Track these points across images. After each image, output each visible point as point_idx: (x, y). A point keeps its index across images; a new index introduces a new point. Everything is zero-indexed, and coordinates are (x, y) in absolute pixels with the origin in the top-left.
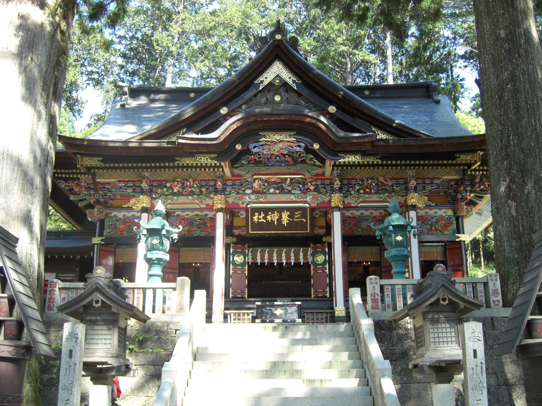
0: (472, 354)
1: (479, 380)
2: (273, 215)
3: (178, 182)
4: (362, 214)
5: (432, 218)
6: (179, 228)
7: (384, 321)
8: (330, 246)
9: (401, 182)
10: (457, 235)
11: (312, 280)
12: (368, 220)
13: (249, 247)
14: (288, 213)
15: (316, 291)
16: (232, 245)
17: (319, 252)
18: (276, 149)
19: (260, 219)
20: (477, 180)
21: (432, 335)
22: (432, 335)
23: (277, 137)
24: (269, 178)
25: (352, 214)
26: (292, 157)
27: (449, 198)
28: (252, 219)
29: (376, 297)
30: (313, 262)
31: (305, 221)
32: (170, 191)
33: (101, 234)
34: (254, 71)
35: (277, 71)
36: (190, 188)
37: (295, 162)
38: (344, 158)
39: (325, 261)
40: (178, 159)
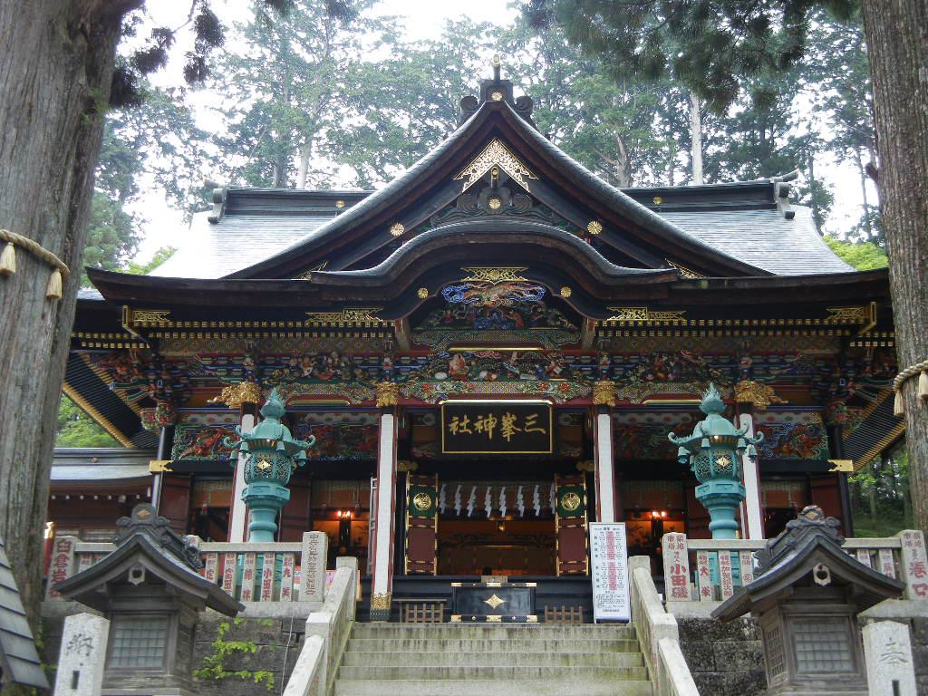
2: (485, 421)
3: (310, 357)
5: (782, 428)
6: (310, 440)
7: (696, 620)
8: (592, 479)
9: (724, 359)
10: (830, 461)
14: (514, 418)
18: (492, 297)
20: (868, 358)
23: (493, 276)
28: (447, 428)
29: (682, 573)
30: (559, 509)
31: (544, 432)
35: (495, 158)
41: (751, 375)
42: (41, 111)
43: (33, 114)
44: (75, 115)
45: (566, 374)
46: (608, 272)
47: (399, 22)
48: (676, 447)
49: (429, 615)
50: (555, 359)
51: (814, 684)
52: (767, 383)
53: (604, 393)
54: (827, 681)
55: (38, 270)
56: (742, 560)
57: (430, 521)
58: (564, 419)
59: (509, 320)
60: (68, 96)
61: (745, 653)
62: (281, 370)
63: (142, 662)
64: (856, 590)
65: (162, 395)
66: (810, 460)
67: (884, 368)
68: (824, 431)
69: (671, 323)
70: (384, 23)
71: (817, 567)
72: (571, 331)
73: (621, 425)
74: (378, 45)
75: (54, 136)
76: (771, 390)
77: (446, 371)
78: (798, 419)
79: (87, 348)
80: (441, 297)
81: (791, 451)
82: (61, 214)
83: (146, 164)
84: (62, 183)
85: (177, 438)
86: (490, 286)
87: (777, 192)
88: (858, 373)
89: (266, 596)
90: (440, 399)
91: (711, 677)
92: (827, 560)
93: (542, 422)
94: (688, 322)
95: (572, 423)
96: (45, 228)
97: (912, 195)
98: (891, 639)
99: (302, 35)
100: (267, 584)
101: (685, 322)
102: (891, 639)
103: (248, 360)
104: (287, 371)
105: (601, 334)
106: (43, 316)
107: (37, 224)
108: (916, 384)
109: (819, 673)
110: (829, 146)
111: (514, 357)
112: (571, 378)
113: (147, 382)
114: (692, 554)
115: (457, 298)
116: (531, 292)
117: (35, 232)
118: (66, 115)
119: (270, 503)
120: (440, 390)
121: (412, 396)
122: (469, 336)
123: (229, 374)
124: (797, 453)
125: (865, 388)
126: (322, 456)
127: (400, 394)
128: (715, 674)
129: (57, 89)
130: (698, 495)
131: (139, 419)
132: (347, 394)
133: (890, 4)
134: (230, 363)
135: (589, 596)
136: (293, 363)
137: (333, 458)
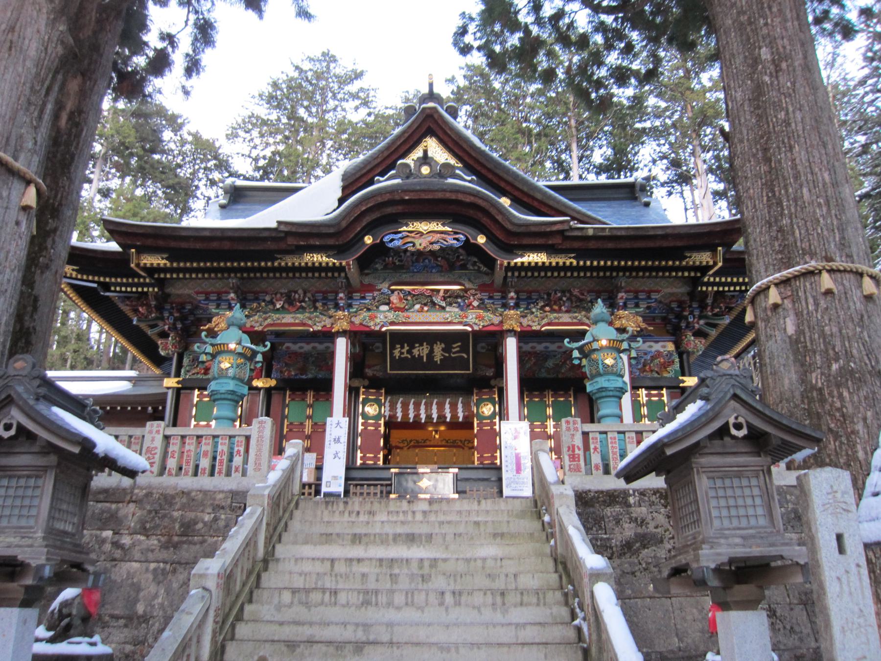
0: (834, 543)
1: (856, 609)
3: (282, 294)
4: (546, 347)
5: (646, 354)
6: (265, 346)
7: (590, 491)
8: (502, 392)
10: (681, 378)
11: (476, 440)
12: (555, 356)
13: (387, 394)
14: (443, 345)
15: (482, 456)
16: (362, 390)
17: (487, 400)
18: (421, 244)
19: (403, 353)
20: (709, 301)
21: (713, 503)
22: (713, 503)
23: (423, 226)
24: (413, 290)
25: (532, 348)
26: (447, 260)
27: (669, 327)
28: (391, 354)
29: (577, 451)
30: (478, 415)
31: (466, 356)
32: (271, 307)
33: (178, 375)
34: (396, 149)
36: (300, 302)
37: (452, 267)
38: (522, 256)
39: (494, 413)
40: (279, 256)
41: (625, 307)
42: (21, 48)
43: (13, 49)
44: (54, 55)
45: (482, 306)
46: (516, 221)
47: (372, 93)
48: (572, 350)
49: (375, 494)
50: (474, 295)
51: (730, 540)
52: (637, 313)
53: (513, 319)
54: (744, 538)
55: (12, 183)
56: (627, 440)
57: (377, 425)
58: (482, 347)
59: (438, 265)
60: (49, 38)
61: (631, 518)
62: (259, 304)
63: (14, 521)
64: (774, 442)
65: (173, 328)
66: (666, 378)
67: (721, 308)
68: (677, 356)
69: (564, 263)
70: (361, 95)
71: (733, 417)
72: (487, 274)
73: (525, 352)
74: (357, 108)
75: (34, 71)
76: (640, 319)
77: (388, 304)
78: (657, 347)
79: (115, 291)
80: (382, 242)
81: (652, 371)
82: (39, 139)
83: (198, 193)
84: (42, 112)
85: (186, 361)
86: (421, 234)
87: (638, 188)
88: (701, 312)
89: (220, 473)
90: (383, 326)
91: (601, 539)
92: (743, 411)
93: (464, 349)
94: (578, 263)
95: (488, 350)
96: (21, 147)
97: (758, 147)
98: (832, 487)
99: (306, 103)
100: (221, 462)
101: (575, 263)
102: (832, 487)
103: (232, 295)
104: (263, 304)
105: (509, 274)
106: (18, 223)
107: (13, 142)
108: (767, 297)
109: (734, 529)
110: (663, 185)
111: (441, 293)
112: (486, 309)
113: (162, 319)
114: (585, 434)
115: (397, 243)
116: (454, 239)
117: (11, 149)
118: (46, 54)
119: (230, 397)
120: (382, 320)
121: (361, 324)
122: (405, 277)
123: (218, 307)
124: (657, 372)
125: (707, 324)
126: (296, 375)
127: (352, 322)
128: (605, 536)
129: (38, 32)
130: (589, 389)
131: (157, 347)
132: (310, 322)
133: (735, 3)
134: (219, 299)
135: (500, 480)
136: (268, 298)
137: (304, 377)
